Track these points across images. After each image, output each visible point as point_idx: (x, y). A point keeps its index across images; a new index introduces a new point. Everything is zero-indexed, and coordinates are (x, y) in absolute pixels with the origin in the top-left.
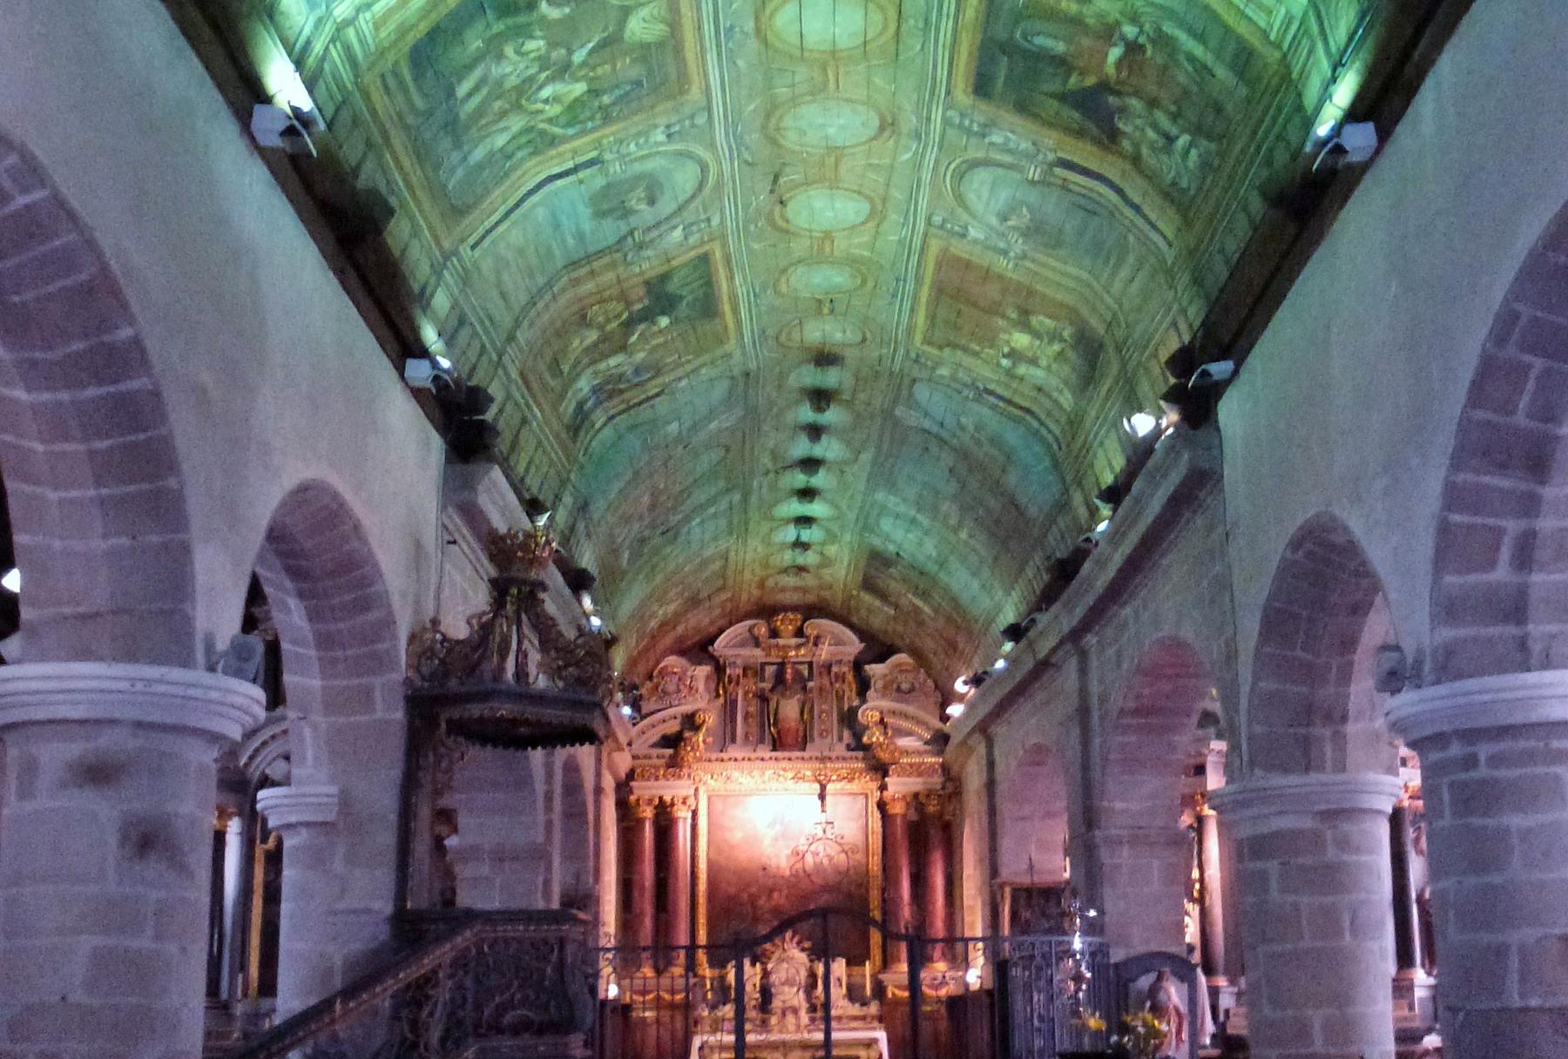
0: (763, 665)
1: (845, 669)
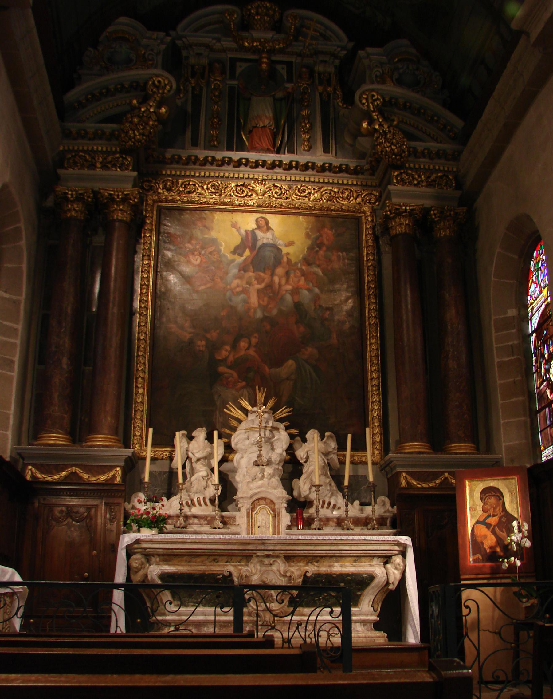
0: (233, 61)
1: (331, 69)
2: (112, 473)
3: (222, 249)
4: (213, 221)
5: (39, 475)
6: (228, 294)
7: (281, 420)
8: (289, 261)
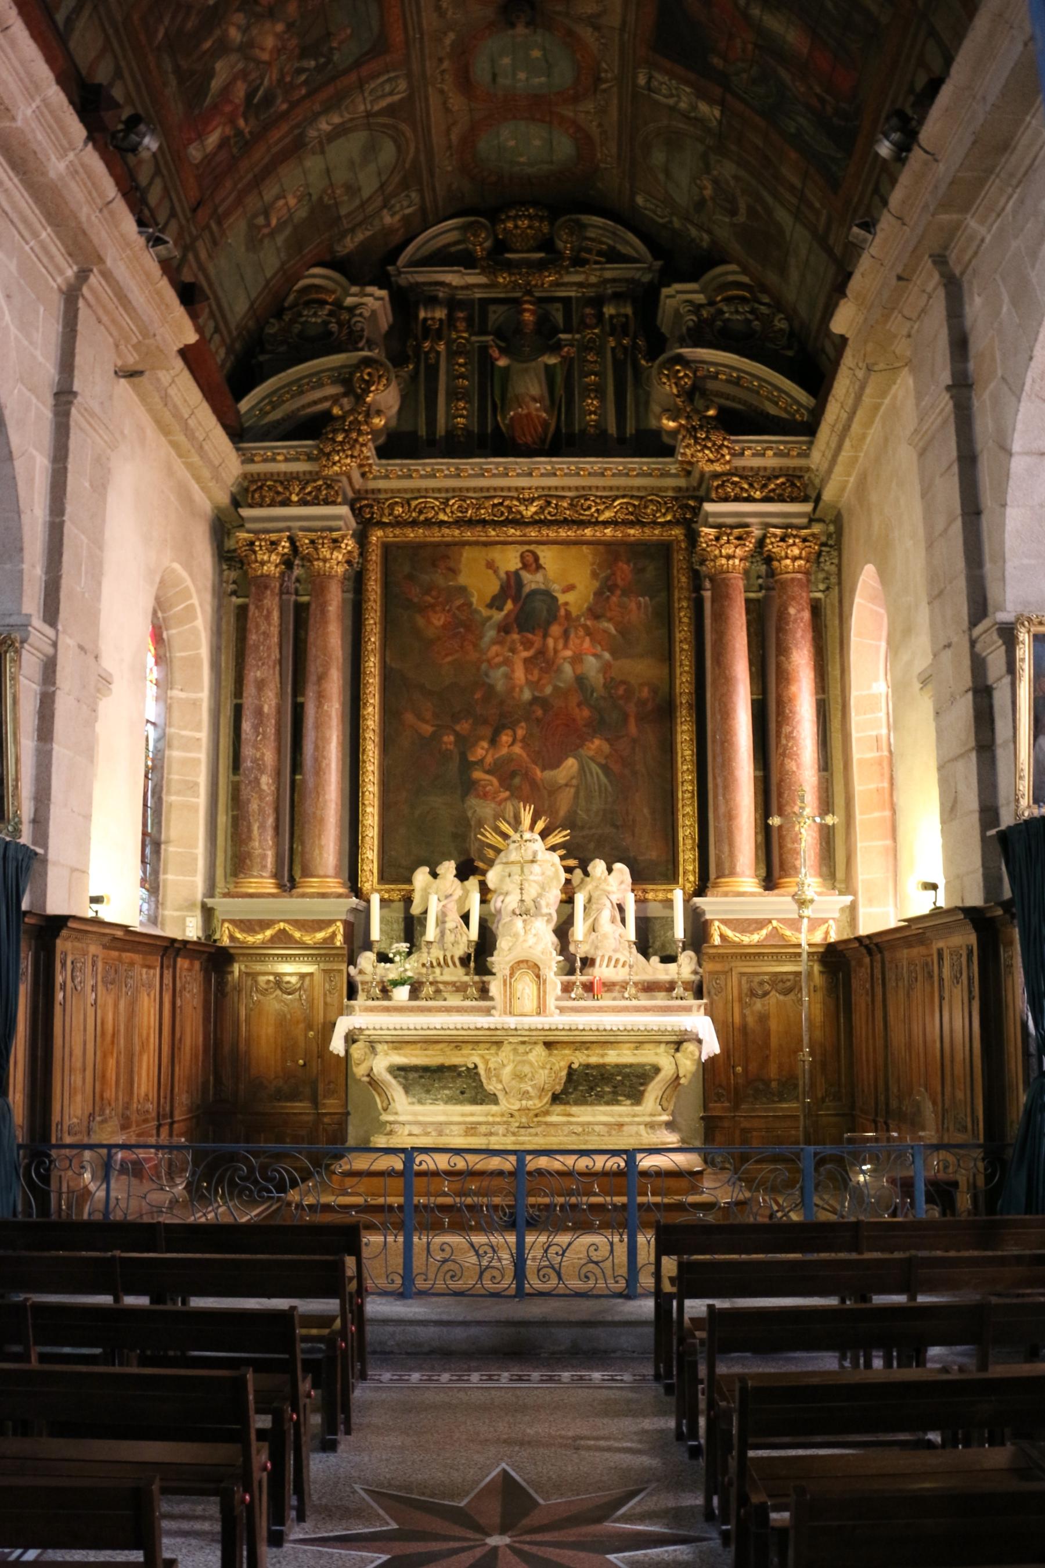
0: (485, 302)
2: (331, 930)
3: (474, 600)
4: (460, 562)
5: (238, 935)
6: (484, 666)
7: (553, 848)
8: (568, 614)
